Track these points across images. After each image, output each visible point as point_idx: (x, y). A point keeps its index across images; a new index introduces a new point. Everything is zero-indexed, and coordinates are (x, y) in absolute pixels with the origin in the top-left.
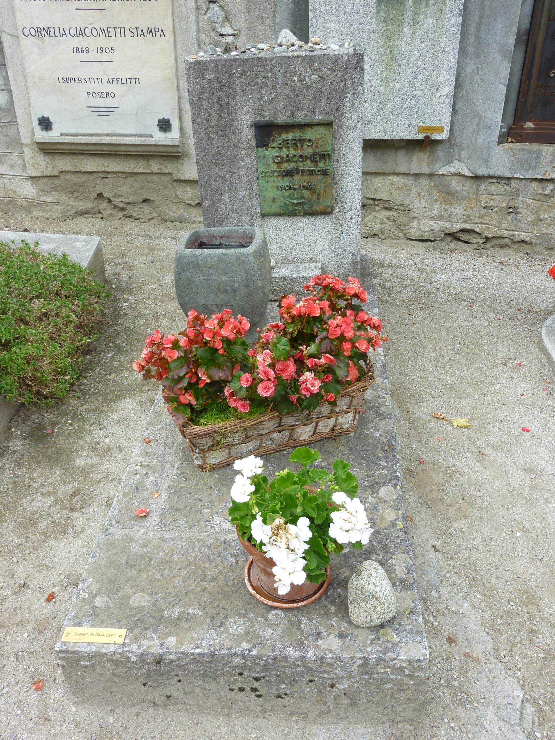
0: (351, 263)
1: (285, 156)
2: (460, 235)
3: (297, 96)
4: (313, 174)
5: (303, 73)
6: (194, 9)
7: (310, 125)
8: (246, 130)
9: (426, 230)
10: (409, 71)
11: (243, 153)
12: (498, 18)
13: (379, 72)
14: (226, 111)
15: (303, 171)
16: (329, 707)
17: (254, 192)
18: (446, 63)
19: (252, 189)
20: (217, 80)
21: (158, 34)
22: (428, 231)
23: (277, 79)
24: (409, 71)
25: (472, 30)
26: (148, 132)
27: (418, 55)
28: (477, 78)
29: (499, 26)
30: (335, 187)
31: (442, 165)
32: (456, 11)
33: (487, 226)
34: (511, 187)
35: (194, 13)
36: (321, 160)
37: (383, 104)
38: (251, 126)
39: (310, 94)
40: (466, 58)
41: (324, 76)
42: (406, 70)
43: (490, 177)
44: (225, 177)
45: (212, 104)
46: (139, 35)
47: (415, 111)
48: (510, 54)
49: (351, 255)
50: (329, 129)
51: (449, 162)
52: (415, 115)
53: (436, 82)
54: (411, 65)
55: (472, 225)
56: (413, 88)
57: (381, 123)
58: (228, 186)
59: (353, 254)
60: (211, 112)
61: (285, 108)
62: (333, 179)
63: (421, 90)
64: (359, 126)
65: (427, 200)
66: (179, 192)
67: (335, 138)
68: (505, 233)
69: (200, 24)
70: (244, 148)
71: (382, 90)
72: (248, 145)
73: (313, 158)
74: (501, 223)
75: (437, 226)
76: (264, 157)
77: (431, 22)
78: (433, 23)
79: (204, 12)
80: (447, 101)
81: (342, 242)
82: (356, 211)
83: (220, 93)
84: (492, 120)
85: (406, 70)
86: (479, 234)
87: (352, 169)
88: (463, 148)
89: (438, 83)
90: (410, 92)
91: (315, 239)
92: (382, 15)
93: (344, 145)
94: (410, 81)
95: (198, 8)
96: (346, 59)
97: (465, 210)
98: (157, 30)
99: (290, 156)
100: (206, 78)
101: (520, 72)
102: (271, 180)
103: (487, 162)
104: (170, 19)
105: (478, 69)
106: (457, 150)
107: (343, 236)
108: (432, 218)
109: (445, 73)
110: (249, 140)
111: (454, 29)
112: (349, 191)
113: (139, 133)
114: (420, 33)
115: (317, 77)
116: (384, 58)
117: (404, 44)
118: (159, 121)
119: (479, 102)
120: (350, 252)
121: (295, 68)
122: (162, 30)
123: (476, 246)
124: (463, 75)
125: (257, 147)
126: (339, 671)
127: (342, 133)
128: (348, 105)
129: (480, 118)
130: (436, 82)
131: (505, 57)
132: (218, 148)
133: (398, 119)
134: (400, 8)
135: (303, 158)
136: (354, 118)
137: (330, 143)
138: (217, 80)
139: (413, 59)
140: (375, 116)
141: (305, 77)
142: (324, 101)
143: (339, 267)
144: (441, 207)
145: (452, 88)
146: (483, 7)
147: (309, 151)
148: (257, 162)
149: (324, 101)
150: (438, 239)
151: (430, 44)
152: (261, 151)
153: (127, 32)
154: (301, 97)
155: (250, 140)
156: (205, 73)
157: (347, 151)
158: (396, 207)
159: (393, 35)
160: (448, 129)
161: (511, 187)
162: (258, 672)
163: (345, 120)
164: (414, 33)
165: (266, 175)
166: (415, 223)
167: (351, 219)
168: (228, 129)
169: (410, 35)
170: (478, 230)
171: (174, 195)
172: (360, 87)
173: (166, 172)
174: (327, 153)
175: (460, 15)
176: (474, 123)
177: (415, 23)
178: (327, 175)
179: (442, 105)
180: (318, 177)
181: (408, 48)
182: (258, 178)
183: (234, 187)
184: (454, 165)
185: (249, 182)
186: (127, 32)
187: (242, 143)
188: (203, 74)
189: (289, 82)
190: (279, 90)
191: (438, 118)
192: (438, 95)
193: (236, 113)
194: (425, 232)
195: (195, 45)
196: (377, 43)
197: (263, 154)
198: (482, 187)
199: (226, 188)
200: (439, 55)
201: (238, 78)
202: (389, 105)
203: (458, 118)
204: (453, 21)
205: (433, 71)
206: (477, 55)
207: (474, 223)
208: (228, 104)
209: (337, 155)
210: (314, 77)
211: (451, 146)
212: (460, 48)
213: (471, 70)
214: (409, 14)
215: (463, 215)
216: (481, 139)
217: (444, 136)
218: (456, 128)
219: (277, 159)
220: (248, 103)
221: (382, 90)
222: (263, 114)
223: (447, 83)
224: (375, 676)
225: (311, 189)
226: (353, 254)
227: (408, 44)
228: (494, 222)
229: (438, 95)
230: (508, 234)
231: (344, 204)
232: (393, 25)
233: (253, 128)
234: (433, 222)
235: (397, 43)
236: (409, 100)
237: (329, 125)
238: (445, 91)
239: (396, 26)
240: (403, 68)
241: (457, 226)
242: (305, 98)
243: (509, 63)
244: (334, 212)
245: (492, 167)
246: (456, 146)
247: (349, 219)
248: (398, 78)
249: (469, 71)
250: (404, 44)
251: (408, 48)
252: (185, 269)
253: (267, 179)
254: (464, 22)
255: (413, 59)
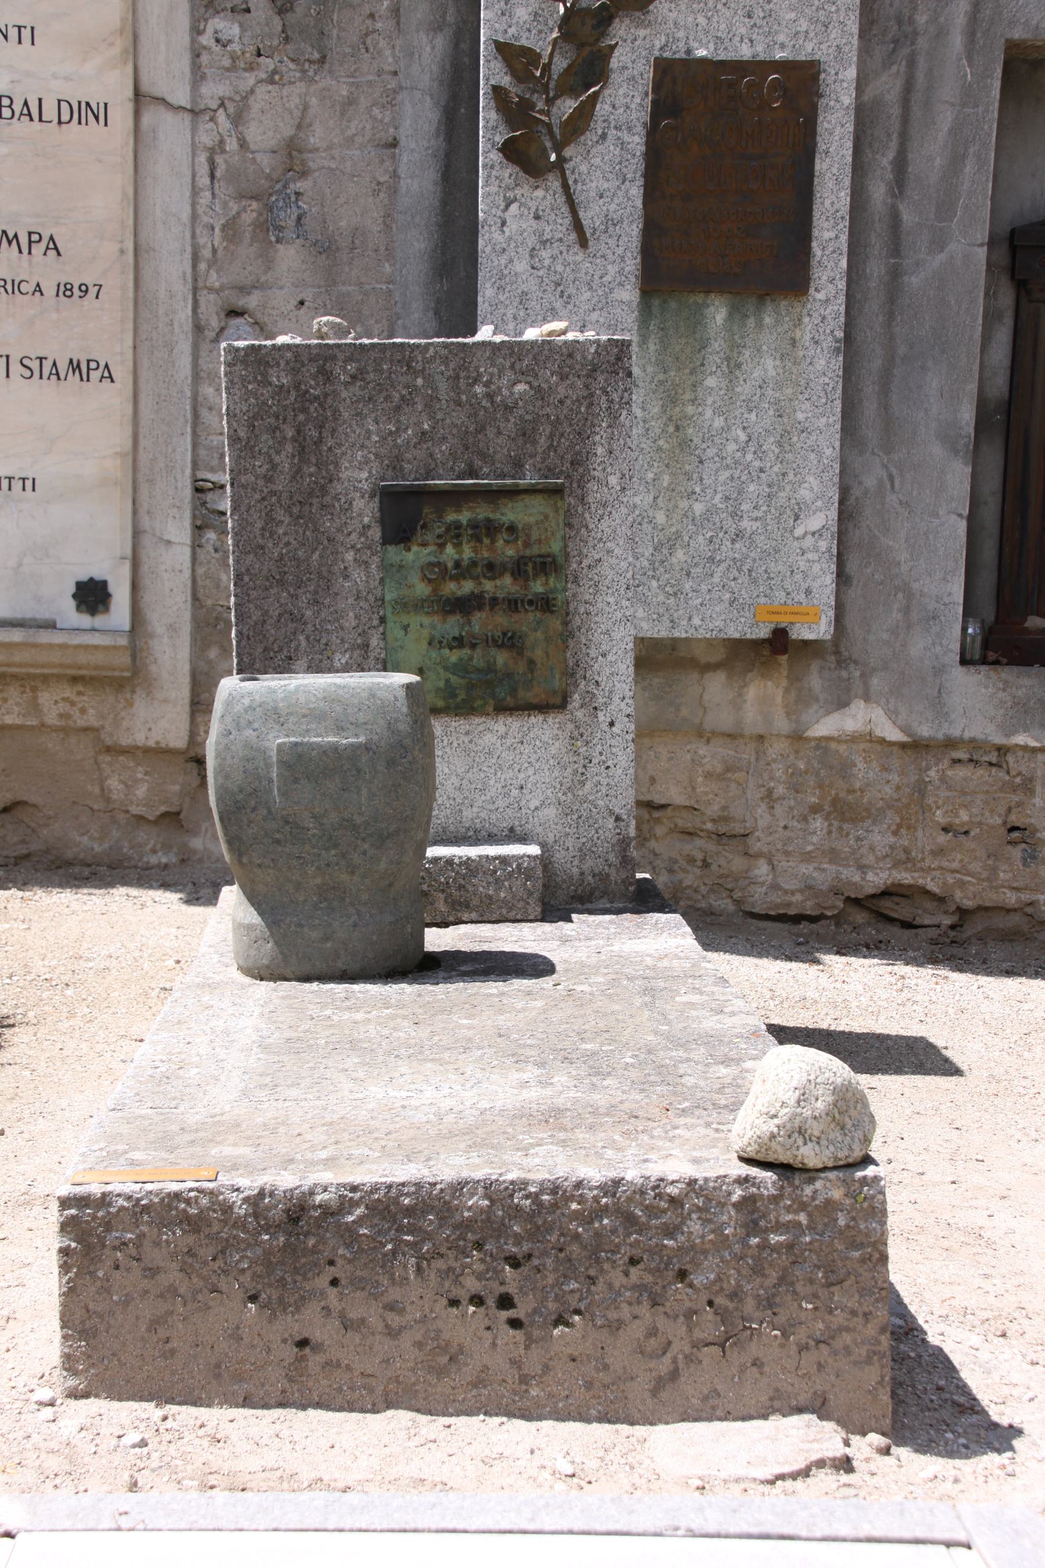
0: (614, 840)
1: (450, 565)
2: (887, 906)
3: (481, 429)
4: (516, 610)
5: (495, 380)
6: (188, 326)
7: (514, 493)
8: (359, 504)
9: (793, 887)
10: (724, 475)
11: (350, 556)
12: (930, 364)
13: (650, 476)
14: (314, 460)
15: (494, 601)
16: (675, 1360)
17: (372, 655)
18: (813, 456)
19: (366, 646)
20: (297, 387)
21: (95, 375)
22: (801, 891)
23: (435, 389)
24: (724, 475)
25: (869, 390)
26: (43, 613)
27: (743, 437)
28: (892, 499)
29: (933, 382)
30: (571, 643)
31: (822, 711)
32: (828, 343)
33: (958, 876)
34: (1008, 773)
35: (190, 335)
36: (536, 576)
37: (665, 551)
38: (372, 496)
39: (510, 426)
40: (861, 453)
41: (545, 386)
42: (717, 471)
43: (950, 743)
44: (303, 616)
45: (283, 441)
46: (46, 373)
47: (745, 568)
48: (966, 445)
49: (612, 820)
50: (556, 503)
51: (842, 704)
52: (746, 579)
53: (793, 501)
54: (729, 461)
55: (916, 875)
56: (736, 515)
57: (661, 598)
58: (307, 638)
59: (618, 819)
60: (277, 459)
61: (453, 455)
62: (566, 624)
63: (756, 519)
64: (625, 500)
65: (791, 808)
66: (114, 783)
67: (569, 525)
68: (1011, 899)
69: (201, 362)
70: (353, 547)
71: (661, 518)
72: (363, 539)
73: (519, 569)
74: (994, 870)
75: (824, 874)
76: (401, 567)
77: (770, 365)
78: (775, 367)
79: (213, 334)
80: (823, 545)
81: (588, 785)
82: (623, 705)
83: (301, 417)
84: (938, 599)
85: (717, 471)
86: (941, 900)
87: (611, 600)
88: (874, 670)
89: (798, 504)
90: (730, 524)
91: (522, 776)
92: (652, 347)
93: (591, 544)
94: (727, 498)
95: (198, 328)
96: (592, 350)
97: (895, 833)
98: (93, 365)
99: (465, 563)
100: (270, 384)
101: (999, 496)
102: (415, 620)
103: (938, 705)
104: (129, 342)
105: (891, 478)
106: (858, 674)
107: (593, 769)
108: (807, 857)
109: (811, 479)
110: (366, 527)
111: (827, 380)
112: (604, 655)
113: (19, 616)
114: (744, 389)
115: (527, 387)
116: (661, 442)
117: (709, 413)
118: (80, 585)
119: (903, 556)
120: (611, 812)
121: (477, 368)
122: (107, 366)
123: (933, 933)
124: (856, 492)
125: (384, 544)
126: (695, 1226)
127: (587, 515)
128: (600, 451)
129: (909, 595)
130: (793, 501)
131: (956, 452)
132: (288, 544)
133: (704, 588)
134: (694, 332)
135: (492, 569)
136: (613, 480)
137: (559, 535)
138: (297, 387)
139: (731, 447)
140: (644, 579)
141: (500, 389)
142: (543, 441)
143: (583, 853)
144: (830, 825)
145: (833, 514)
146: (892, 338)
147: (507, 551)
148: (382, 581)
149: (543, 441)
150: (829, 913)
151: (771, 413)
152: (394, 553)
153: (16, 368)
154: (491, 432)
155: (369, 527)
156: (271, 371)
157: (597, 557)
158: (709, 826)
159: (680, 391)
160: (831, 613)
161: (1008, 773)
162: (518, 1240)
163: (592, 486)
164: (730, 388)
165: (404, 605)
166: (762, 870)
167: (612, 724)
168: (315, 501)
169: (722, 392)
170: (932, 887)
171: (97, 790)
172: (624, 412)
173: (81, 723)
174: (550, 559)
175: (837, 350)
176: (896, 606)
177: (733, 367)
178: (552, 612)
179: (810, 556)
180: (531, 616)
181: (719, 422)
182: (383, 620)
183: (323, 641)
184: (853, 712)
185: (360, 630)
186: (16, 368)
187: (349, 534)
188: (265, 375)
189: (464, 397)
190: (440, 416)
191: (804, 586)
192: (799, 531)
193: (337, 465)
194: (793, 893)
195: (188, 407)
196: (644, 409)
197: (398, 559)
198: (932, 773)
199: (304, 644)
200: (795, 439)
201: (346, 384)
202: (680, 555)
203: (853, 594)
204: (823, 362)
205: (784, 475)
206: (888, 447)
207: (922, 870)
208: (319, 442)
209: (575, 566)
210: (521, 387)
211: (842, 663)
212: (843, 429)
213: (875, 482)
214: (717, 345)
215: (891, 847)
216: (918, 646)
217: (821, 629)
218: (851, 621)
219: (432, 572)
220: (367, 443)
221: (661, 518)
222: (402, 469)
223: (819, 503)
224: (775, 1238)
225: (513, 646)
226: (618, 819)
227: (717, 412)
228: (975, 866)
229: (799, 531)
230: (1019, 900)
231: (592, 688)
232: (679, 369)
233: (377, 499)
234: (811, 868)
235: (690, 409)
236: (728, 543)
237: (557, 491)
238: (815, 522)
239: (687, 371)
240: (709, 467)
241: (877, 879)
242: (499, 433)
243: (966, 464)
244: (569, 707)
245: (953, 716)
246: (856, 662)
247: (605, 727)
248: (698, 490)
249: (870, 482)
250: (709, 413)
251: (719, 422)
252: (243, 723)
253: (405, 619)
254: (848, 370)
255: (731, 447)
